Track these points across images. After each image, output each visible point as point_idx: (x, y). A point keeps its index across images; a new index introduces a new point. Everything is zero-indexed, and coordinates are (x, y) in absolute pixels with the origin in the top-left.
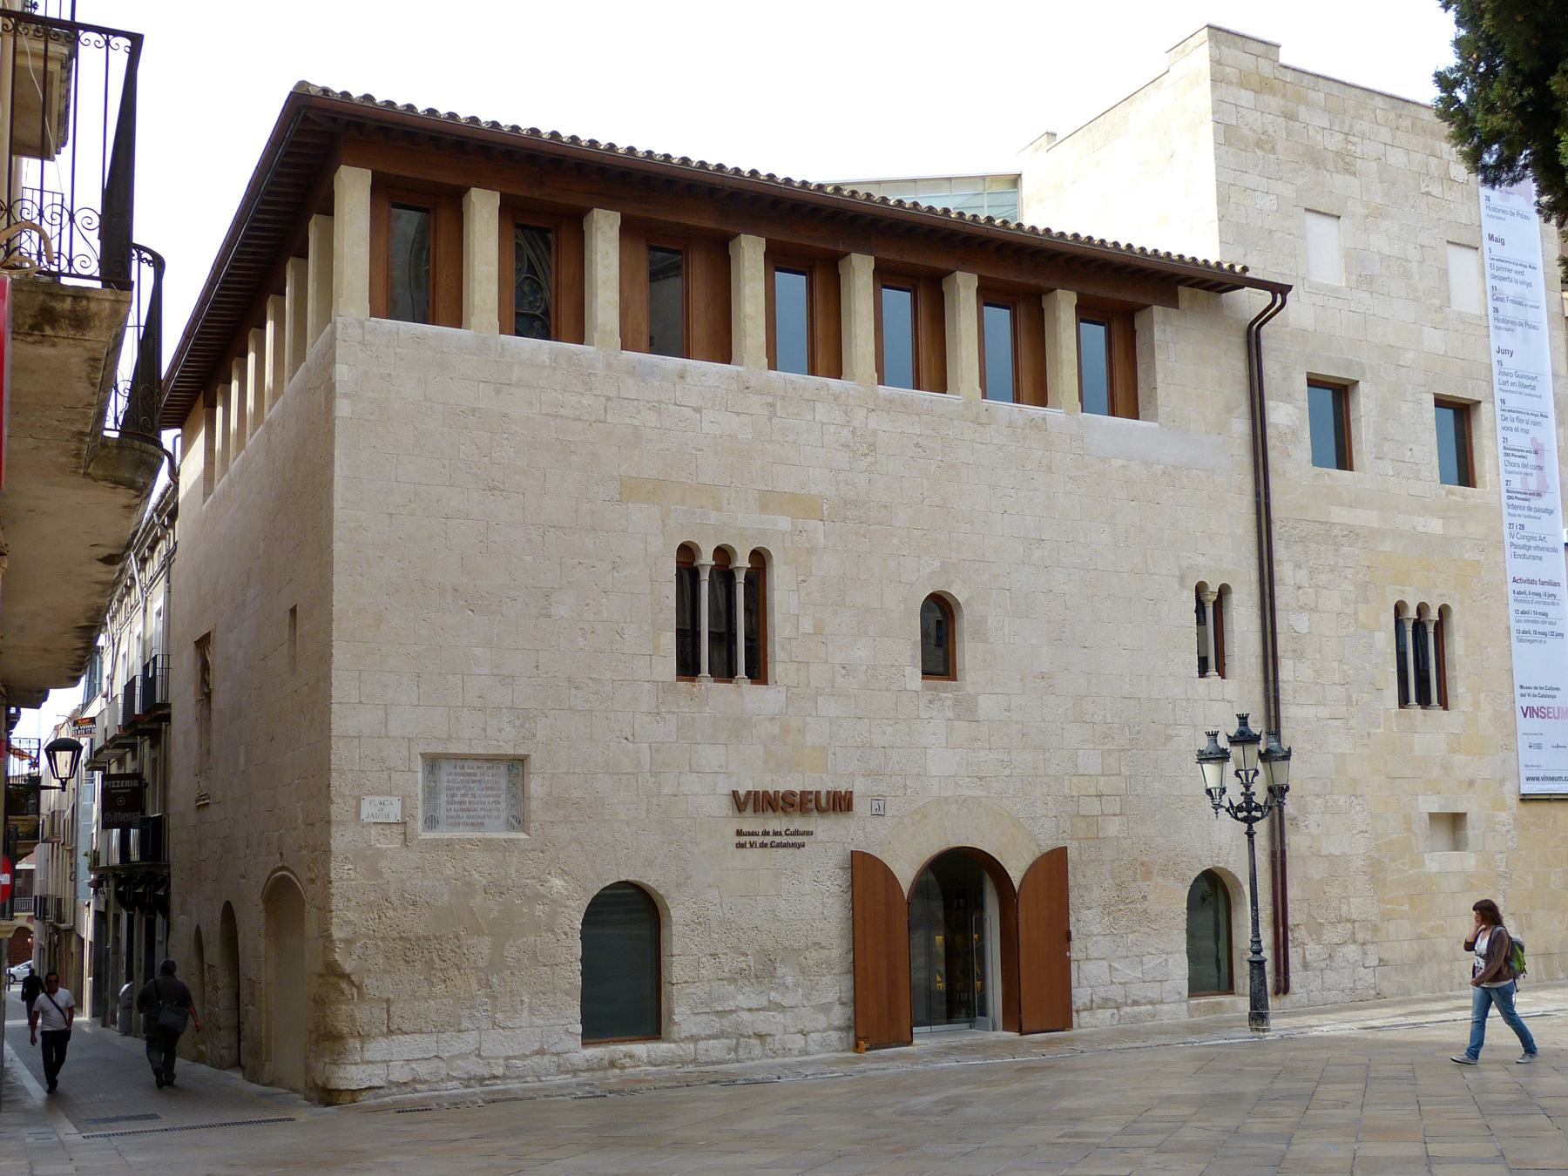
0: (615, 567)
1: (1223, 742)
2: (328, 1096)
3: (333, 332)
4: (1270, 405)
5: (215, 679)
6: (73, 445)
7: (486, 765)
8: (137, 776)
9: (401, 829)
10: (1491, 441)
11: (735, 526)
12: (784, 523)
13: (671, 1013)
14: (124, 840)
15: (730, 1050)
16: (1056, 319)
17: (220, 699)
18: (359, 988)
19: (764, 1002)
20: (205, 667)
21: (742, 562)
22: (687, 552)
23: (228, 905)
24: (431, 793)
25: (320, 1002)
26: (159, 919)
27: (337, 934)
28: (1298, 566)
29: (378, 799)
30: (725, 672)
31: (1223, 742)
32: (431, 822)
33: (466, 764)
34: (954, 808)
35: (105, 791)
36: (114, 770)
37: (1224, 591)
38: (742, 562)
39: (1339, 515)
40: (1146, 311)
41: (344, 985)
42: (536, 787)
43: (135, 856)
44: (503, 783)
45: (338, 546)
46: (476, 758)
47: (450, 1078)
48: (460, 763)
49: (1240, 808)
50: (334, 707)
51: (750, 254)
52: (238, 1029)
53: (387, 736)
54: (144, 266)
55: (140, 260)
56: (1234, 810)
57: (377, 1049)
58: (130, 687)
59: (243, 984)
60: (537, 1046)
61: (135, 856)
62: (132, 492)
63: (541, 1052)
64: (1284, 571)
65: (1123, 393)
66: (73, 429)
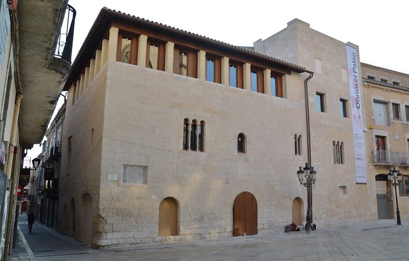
0: (170, 123)
1: (303, 169)
2: (97, 247)
3: (107, 64)
4: (309, 97)
6: (45, 54)
7: (138, 168)
8: (53, 169)
11: (196, 115)
12: (208, 115)
13: (179, 229)
14: (49, 183)
15: (193, 237)
16: (266, 75)
18: (106, 221)
19: (201, 226)
20: (70, 144)
22: (186, 120)
23: (73, 199)
24: (125, 174)
25: (96, 224)
26: (56, 202)
27: (100, 207)
28: (314, 132)
30: (194, 148)
31: (303, 169)
34: (244, 182)
35: (45, 172)
36: (47, 167)
38: (199, 123)
41: (102, 220)
42: (149, 173)
43: (51, 187)
45: (105, 114)
46: (135, 166)
47: (127, 243)
49: (306, 184)
50: (103, 152)
51: (202, 55)
52: (74, 228)
54: (70, 12)
55: (70, 10)
56: (305, 184)
57: (109, 236)
58: (52, 148)
59: (76, 217)
60: (148, 236)
61: (51, 187)
62: (61, 75)
63: (148, 238)
64: (312, 133)
66: (46, 46)
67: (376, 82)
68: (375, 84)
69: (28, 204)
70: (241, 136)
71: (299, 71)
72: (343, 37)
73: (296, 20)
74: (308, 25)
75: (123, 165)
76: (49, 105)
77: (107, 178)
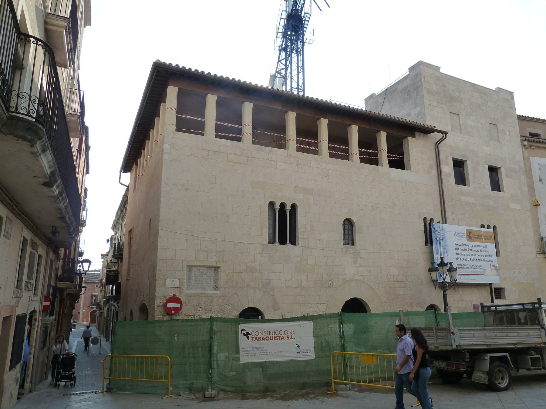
5: (133, 242)
9: (179, 289)
10: (505, 180)
12: (301, 196)
17: (133, 248)
21: (288, 208)
22: (272, 204)
23: (131, 310)
24: (189, 278)
29: (171, 280)
30: (282, 241)
32: (189, 287)
33: (201, 268)
37: (432, 220)
38: (288, 208)
39: (463, 198)
40: (406, 139)
42: (223, 276)
43: (114, 294)
44: (213, 275)
48: (199, 268)
50: (159, 250)
53: (175, 259)
61: (114, 294)
65: (398, 162)
67: (541, 141)
68: (540, 142)
69: (97, 314)
70: (349, 224)
71: (426, 131)
72: (490, 83)
73: (420, 63)
74: (438, 68)
75: (187, 266)
76: (44, 189)
77: (165, 284)
